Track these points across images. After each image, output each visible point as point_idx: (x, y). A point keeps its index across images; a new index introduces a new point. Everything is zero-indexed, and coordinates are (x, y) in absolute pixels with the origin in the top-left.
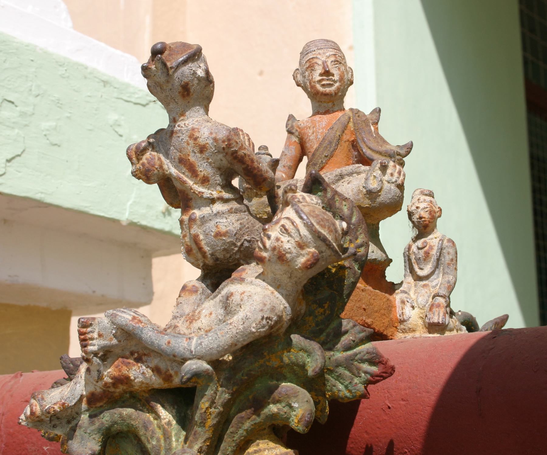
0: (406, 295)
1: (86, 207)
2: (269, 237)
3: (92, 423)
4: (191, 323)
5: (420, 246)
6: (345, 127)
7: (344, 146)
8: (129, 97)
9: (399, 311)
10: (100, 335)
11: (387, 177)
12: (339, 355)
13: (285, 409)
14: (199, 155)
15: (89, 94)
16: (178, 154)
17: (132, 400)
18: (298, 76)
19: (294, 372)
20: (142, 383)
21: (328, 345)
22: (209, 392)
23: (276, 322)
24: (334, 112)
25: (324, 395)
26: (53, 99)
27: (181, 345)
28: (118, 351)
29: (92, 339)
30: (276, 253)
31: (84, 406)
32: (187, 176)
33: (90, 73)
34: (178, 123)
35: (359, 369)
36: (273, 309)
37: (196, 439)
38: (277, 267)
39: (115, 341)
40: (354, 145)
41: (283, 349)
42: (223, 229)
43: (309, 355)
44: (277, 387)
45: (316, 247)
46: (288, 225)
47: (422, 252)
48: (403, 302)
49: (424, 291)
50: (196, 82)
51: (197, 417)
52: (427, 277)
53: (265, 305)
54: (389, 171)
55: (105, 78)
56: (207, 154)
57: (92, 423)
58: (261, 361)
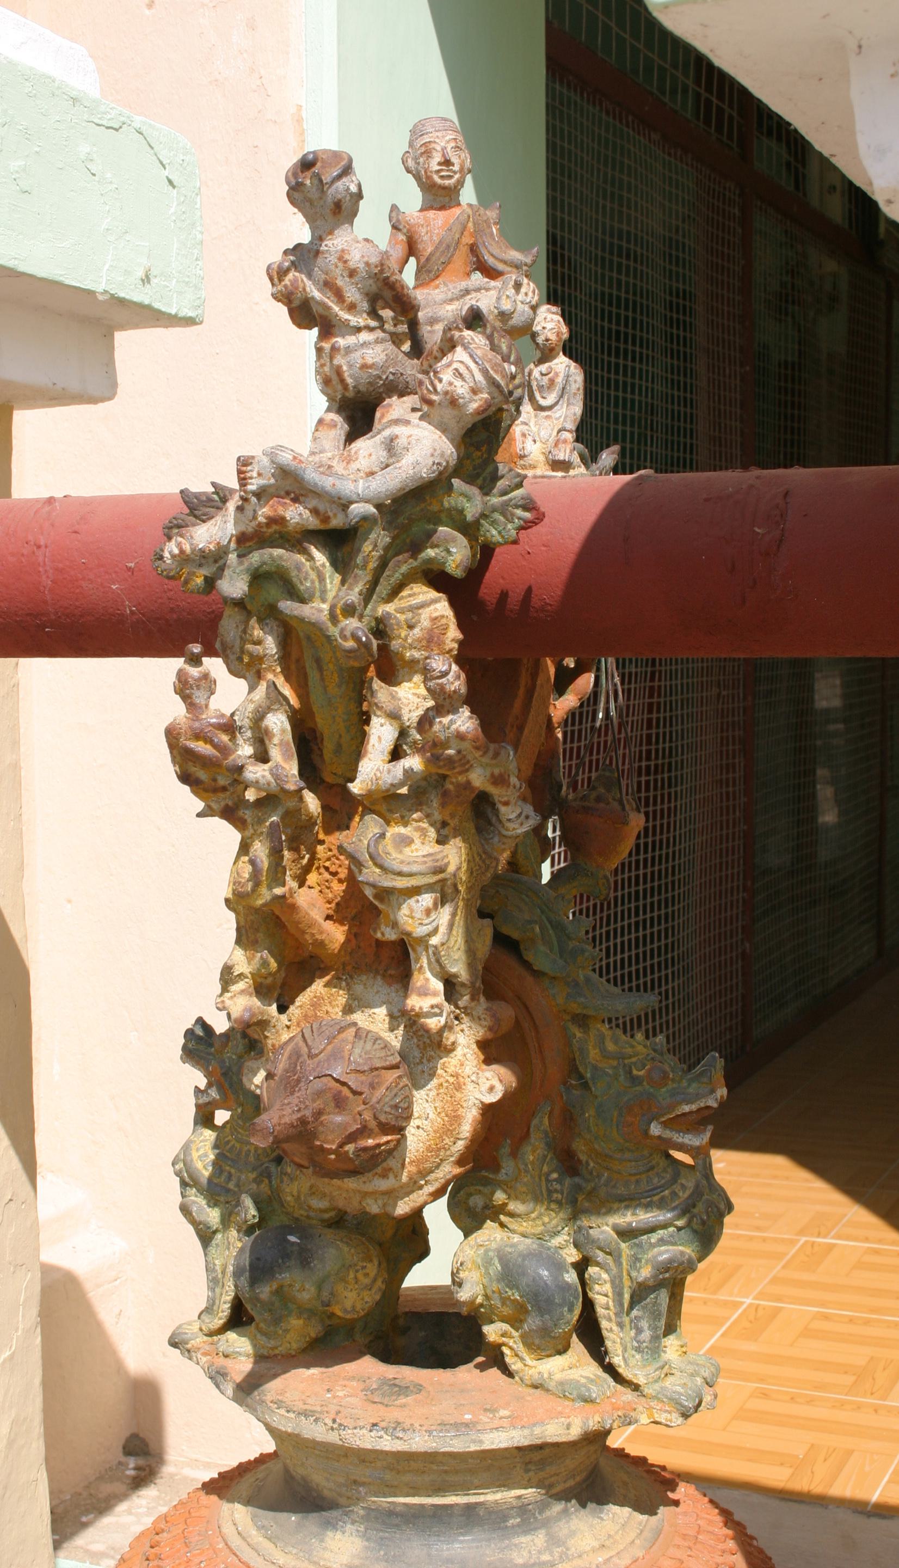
0: (527, 427)
1: (61, 275)
2: (440, 381)
3: (241, 563)
4: (348, 463)
5: (544, 372)
6: (464, 228)
7: (464, 250)
8: (100, 119)
9: (519, 445)
10: (259, 475)
11: (520, 297)
12: (495, 500)
13: (443, 554)
14: (348, 280)
15: (57, 118)
16: (323, 276)
17: (280, 541)
18: (409, 160)
19: (450, 516)
20: (298, 523)
21: (486, 489)
22: (373, 536)
23: (446, 468)
24: (450, 207)
25: (477, 540)
26: (21, 128)
27: (348, 488)
28: (272, 490)
29: (251, 478)
30: (448, 397)
31: (233, 545)
32: (332, 301)
33: (59, 88)
34: (326, 243)
35: (513, 515)
36: (442, 455)
37: (356, 582)
38: (447, 412)
39: (272, 481)
40: (473, 249)
41: (444, 494)
42: (370, 361)
43: (466, 497)
44: (435, 531)
45: (489, 393)
46: (462, 369)
47: (546, 379)
48: (524, 435)
49: (547, 423)
50: (348, 198)
51: (359, 560)
52: (550, 408)
53: (435, 450)
54: (523, 290)
55: (74, 94)
56: (356, 279)
57: (241, 563)
58: (423, 505)
